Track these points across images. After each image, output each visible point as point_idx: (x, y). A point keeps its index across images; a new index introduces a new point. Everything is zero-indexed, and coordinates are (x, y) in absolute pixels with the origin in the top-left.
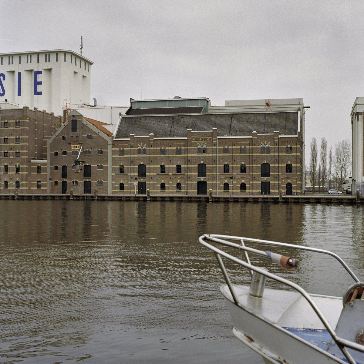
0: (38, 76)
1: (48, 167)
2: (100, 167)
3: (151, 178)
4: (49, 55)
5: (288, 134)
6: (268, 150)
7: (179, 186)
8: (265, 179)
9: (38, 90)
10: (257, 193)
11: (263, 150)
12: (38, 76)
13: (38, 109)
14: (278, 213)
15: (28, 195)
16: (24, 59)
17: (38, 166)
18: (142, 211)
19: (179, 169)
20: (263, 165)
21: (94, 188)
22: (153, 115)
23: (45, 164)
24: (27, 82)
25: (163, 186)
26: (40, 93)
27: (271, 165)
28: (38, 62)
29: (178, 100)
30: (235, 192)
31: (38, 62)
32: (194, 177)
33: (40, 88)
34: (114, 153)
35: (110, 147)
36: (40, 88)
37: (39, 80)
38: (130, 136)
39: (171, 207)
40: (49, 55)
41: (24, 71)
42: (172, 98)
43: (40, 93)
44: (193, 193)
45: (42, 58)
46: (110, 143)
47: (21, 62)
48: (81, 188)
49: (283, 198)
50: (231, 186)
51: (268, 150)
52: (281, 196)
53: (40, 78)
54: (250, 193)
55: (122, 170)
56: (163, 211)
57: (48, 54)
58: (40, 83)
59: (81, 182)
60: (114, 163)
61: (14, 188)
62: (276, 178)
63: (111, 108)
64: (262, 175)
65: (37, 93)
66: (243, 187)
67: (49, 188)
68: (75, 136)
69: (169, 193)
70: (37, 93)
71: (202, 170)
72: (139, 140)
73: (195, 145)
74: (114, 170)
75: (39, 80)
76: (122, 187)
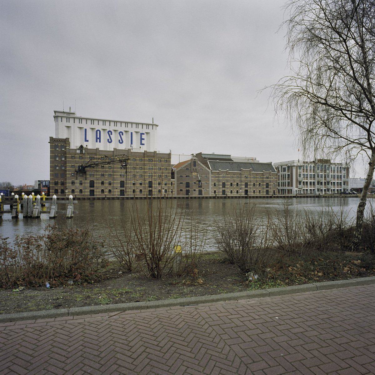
0: (143, 135)
3: (227, 188)
4: (69, 119)
5: (255, 171)
7: (237, 192)
11: (223, 177)
12: (143, 135)
13: (100, 149)
14: (195, 204)
15: (140, 196)
16: (145, 126)
18: (122, 205)
20: (267, 183)
21: (203, 193)
22: (218, 161)
23: (174, 181)
24: (136, 138)
25: (231, 192)
28: (74, 122)
33: (143, 142)
36: (143, 142)
38: (263, 172)
39: (107, 203)
41: (78, 128)
42: (211, 153)
43: (88, 141)
44: (243, 194)
45: (134, 125)
48: (197, 192)
50: (233, 191)
53: (143, 137)
55: (215, 185)
56: (224, 204)
57: (148, 125)
59: (197, 190)
62: (227, 188)
64: (121, 187)
65: (142, 144)
68: (195, 169)
69: (256, 194)
70: (142, 144)
71: (246, 185)
72: (223, 172)
73: (244, 175)
74: (212, 184)
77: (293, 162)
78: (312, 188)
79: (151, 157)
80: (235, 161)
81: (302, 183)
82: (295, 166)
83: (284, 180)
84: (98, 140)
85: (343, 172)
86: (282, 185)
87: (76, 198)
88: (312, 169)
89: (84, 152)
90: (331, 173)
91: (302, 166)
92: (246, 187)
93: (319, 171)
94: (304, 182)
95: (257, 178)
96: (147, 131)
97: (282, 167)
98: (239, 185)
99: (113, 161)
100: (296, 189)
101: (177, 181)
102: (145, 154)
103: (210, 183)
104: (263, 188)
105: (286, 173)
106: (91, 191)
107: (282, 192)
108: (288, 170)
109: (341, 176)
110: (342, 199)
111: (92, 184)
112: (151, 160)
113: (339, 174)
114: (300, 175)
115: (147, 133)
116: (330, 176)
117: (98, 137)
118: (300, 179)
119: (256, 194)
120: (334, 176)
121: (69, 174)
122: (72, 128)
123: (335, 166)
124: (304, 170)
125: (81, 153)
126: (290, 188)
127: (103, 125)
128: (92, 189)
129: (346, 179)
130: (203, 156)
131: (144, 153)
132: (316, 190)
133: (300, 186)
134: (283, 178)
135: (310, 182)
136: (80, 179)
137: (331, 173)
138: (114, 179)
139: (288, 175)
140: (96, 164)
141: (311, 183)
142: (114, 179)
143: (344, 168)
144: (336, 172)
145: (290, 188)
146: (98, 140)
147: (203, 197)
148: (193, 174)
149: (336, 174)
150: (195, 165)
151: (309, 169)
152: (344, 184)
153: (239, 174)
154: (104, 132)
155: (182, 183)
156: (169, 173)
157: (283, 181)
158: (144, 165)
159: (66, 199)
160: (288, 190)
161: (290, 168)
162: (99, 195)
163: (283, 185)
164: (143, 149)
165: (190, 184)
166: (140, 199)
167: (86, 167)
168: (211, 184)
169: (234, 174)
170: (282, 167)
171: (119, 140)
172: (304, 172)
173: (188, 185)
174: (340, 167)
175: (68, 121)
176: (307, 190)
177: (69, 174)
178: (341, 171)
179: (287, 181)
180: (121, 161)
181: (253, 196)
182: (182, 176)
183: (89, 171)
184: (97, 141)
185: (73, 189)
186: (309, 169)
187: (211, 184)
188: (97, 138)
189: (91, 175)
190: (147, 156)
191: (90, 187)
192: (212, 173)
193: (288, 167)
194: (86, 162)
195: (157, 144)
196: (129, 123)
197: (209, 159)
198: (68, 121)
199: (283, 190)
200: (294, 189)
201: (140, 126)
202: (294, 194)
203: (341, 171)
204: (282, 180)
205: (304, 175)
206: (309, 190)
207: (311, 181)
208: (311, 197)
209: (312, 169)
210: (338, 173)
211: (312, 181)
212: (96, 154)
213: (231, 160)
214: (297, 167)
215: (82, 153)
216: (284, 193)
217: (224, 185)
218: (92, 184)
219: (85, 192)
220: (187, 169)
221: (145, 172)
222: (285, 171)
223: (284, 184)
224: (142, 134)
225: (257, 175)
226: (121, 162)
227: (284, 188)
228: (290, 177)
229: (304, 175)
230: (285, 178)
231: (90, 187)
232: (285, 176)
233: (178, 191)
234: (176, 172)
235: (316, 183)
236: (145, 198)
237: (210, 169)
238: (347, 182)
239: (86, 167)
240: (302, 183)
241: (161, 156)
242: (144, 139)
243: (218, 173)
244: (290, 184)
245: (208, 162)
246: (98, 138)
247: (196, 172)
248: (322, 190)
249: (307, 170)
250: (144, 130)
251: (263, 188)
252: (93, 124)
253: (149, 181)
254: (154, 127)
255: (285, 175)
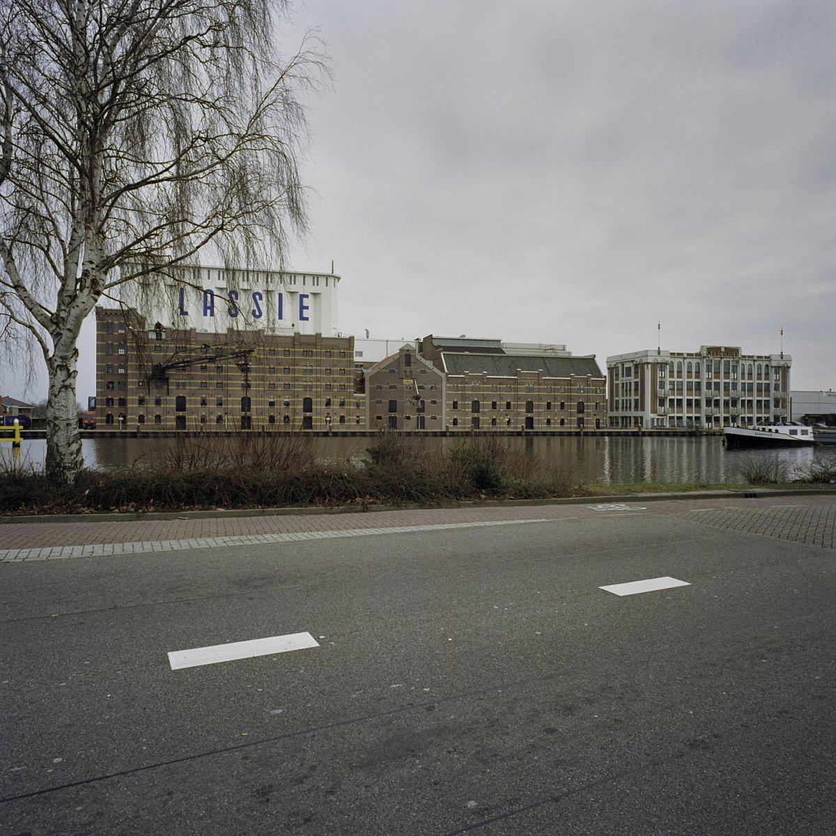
0: (305, 299)
1: (367, 401)
2: (434, 402)
3: (484, 413)
4: (318, 278)
5: (552, 376)
6: (478, 389)
7: (562, 422)
8: (581, 416)
9: (304, 316)
10: (575, 428)
11: (473, 389)
12: (305, 299)
13: (323, 336)
16: (309, 280)
17: (597, 404)
18: (530, 445)
19: (508, 405)
22: (466, 353)
23: (364, 398)
24: (290, 308)
26: (307, 319)
27: (481, 403)
29: (463, 339)
30: (557, 428)
31: (304, 284)
32: (522, 413)
33: (306, 313)
34: (448, 388)
35: (444, 383)
36: (306, 313)
37: (305, 304)
38: (571, 376)
39: (556, 441)
40: (318, 278)
42: (457, 336)
43: (307, 319)
46: (444, 379)
47: (306, 283)
49: (526, 432)
51: (478, 389)
52: (523, 430)
53: (306, 302)
54: (568, 428)
55: (455, 405)
56: (580, 449)
57: (316, 277)
58: (307, 308)
59: (414, 417)
60: (448, 399)
61: (137, 423)
62: (484, 413)
63: (387, 341)
65: (302, 318)
66: (562, 422)
67: (368, 423)
69: (554, 428)
71: (530, 407)
72: (473, 378)
73: (524, 384)
74: (448, 405)
75: (305, 304)
76: (455, 422)
77: (646, 354)
78: (694, 415)
79: (311, 345)
80: (508, 353)
81: (667, 404)
82: (648, 363)
83: (627, 396)
84: (209, 311)
85: (773, 376)
86: (623, 408)
87: (139, 433)
88: (694, 371)
89: (164, 336)
90: (743, 378)
91: (667, 364)
92: (528, 411)
93: (712, 375)
94: (743, 402)
95: (555, 390)
96: (316, 289)
97: (623, 365)
98: (512, 406)
99: (219, 355)
100: (653, 416)
101: (371, 398)
102: (297, 339)
103: (444, 403)
104: (571, 414)
105: (632, 379)
106: (178, 418)
107: (623, 423)
108: (636, 372)
109: (699, 384)
110: (620, 441)
111: (181, 404)
112: (310, 353)
113: (764, 381)
114: (662, 385)
115: (315, 294)
116: (739, 387)
117: (209, 305)
118: (661, 393)
119: (554, 428)
120: (751, 385)
121: (133, 383)
122: (323, 296)
123: (681, 360)
124: (671, 372)
125: (157, 339)
126: (639, 414)
127: (314, 285)
128: (308, 414)
129: (780, 394)
130: (436, 343)
131: (294, 337)
132: (704, 419)
133: (661, 410)
134: (626, 391)
135: (688, 400)
136: (155, 393)
137: (743, 378)
138: (228, 394)
139: (636, 383)
140: (188, 362)
141: (689, 402)
142: (228, 394)
143: (777, 368)
144: (685, 374)
145: (639, 414)
146: (209, 311)
147: (426, 434)
148: (405, 382)
149: (755, 381)
150: (408, 363)
151: (685, 370)
152: (776, 405)
153: (566, 383)
154: (315, 298)
155: (381, 402)
156: (349, 380)
157: (625, 398)
158: (294, 363)
159: (664, 434)
160: (636, 418)
161: (639, 367)
162: (102, 427)
163: (626, 408)
164: (307, 329)
165: (397, 404)
166: (433, 436)
167: (168, 368)
168: (446, 404)
169: (501, 381)
170: (623, 365)
171: (254, 311)
172: (672, 376)
173: (393, 407)
174: (767, 366)
175: (293, 282)
176: (680, 418)
177: (133, 383)
178: (767, 374)
179: (633, 398)
180: (236, 355)
181: (559, 430)
182: (380, 387)
183: (175, 377)
184: (205, 314)
185: (141, 414)
186: (685, 370)
187: (446, 404)
188: (206, 308)
189: (178, 385)
190: (301, 345)
191: (178, 409)
192: (448, 379)
193: (636, 366)
194: (168, 358)
195: (336, 318)
196: (308, 275)
197: (446, 348)
198: (293, 282)
199: (626, 417)
200: (648, 415)
201: (300, 279)
202: (647, 426)
203: (767, 374)
204: (623, 396)
205: (672, 383)
206: (685, 419)
207: (690, 398)
208: (675, 434)
209: (694, 371)
210: (759, 378)
211: (694, 398)
212: (315, 345)
213: (500, 350)
214: (654, 365)
215: (161, 339)
216: (626, 426)
217: (476, 407)
218: (181, 404)
219: (210, 421)
220: (392, 371)
221: (296, 379)
222: (629, 375)
223: (626, 407)
224: (302, 297)
225: (555, 385)
226: (237, 357)
227: (627, 414)
228: (640, 388)
229: (672, 383)
230: (630, 390)
231: (178, 409)
232: (630, 386)
233: (371, 419)
234: (367, 379)
235: (703, 403)
236: (519, 434)
237: (442, 370)
238: (784, 401)
239: (168, 368)
240: (667, 404)
241: (333, 343)
242: (307, 308)
243: (463, 381)
244: (640, 405)
245: (442, 356)
246: (209, 308)
247: (412, 379)
248: (717, 419)
249: (680, 372)
250: (309, 288)
251: (571, 414)
252: (318, 285)
253: (305, 397)
254: (331, 281)
255: (630, 383)
